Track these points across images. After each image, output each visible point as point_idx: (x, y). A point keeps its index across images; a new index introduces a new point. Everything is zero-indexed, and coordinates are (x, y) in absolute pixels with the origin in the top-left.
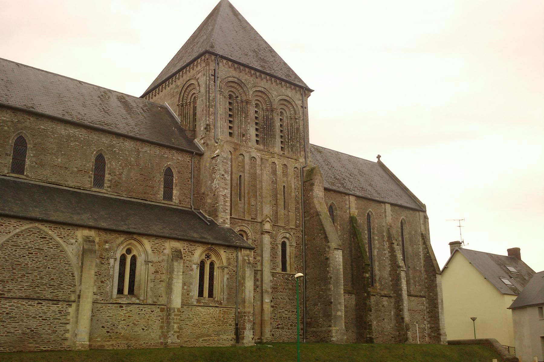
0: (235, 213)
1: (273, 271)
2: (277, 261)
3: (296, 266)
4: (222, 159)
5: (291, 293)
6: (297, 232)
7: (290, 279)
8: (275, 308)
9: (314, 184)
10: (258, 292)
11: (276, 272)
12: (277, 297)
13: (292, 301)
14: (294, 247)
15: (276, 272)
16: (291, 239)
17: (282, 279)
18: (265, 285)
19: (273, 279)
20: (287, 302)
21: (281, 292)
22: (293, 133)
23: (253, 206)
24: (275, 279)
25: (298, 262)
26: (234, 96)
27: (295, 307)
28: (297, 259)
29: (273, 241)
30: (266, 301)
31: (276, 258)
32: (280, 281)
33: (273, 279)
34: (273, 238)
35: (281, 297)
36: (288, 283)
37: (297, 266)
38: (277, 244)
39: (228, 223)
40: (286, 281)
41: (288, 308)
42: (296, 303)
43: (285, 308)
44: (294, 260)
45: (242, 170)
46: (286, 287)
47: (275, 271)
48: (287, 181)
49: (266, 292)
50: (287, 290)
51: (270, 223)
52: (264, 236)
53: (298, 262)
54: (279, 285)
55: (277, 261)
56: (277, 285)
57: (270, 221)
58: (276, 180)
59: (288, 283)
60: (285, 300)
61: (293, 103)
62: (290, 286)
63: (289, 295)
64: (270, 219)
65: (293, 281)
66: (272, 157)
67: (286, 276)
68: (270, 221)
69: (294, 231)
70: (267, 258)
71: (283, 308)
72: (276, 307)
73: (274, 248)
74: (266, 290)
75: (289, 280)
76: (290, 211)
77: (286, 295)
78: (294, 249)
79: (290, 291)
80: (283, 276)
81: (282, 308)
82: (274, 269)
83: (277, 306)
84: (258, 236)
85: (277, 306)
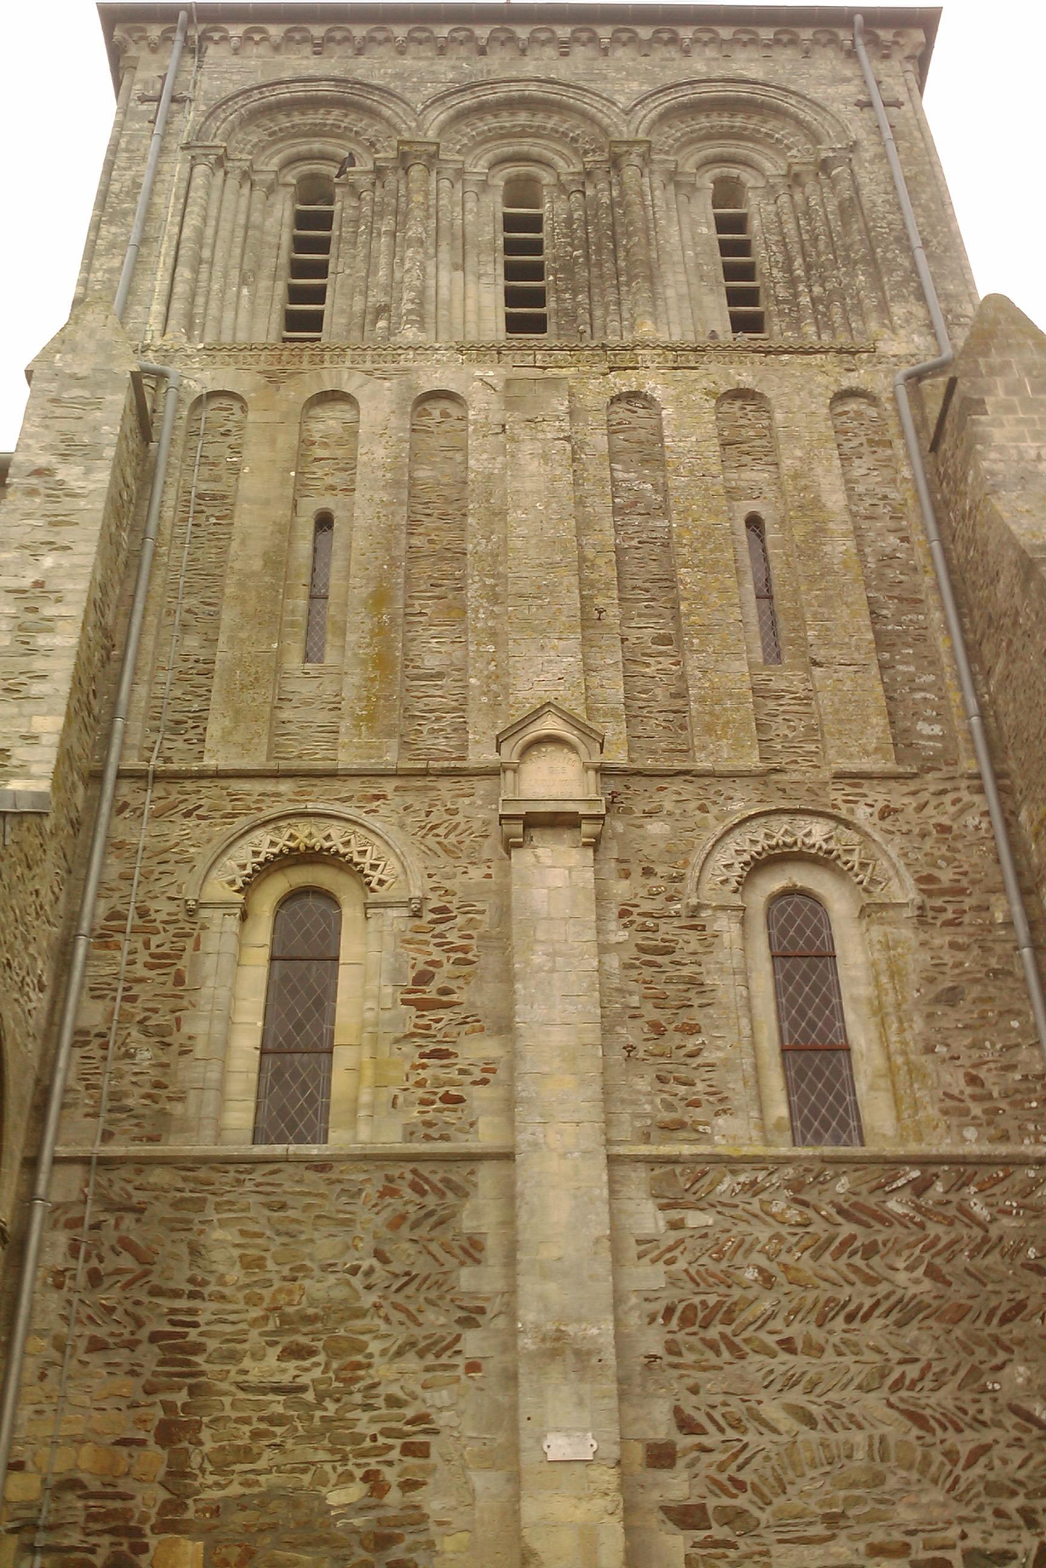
0: (238, 737)
1: (666, 1150)
2: (707, 1056)
3: (955, 1080)
4: (53, 386)
5: (926, 1351)
6: (925, 796)
7: (894, 1205)
8: (719, 1532)
9: (982, 402)
10: (473, 1367)
11: (696, 1159)
12: (736, 1407)
13: (965, 1443)
14: (908, 912)
15: (703, 1149)
16: (855, 859)
17: (793, 1214)
18: (551, 1287)
19: (676, 1225)
20: (881, 1449)
21: (788, 1345)
22: (815, 240)
23: (440, 675)
24: (695, 1219)
25: (977, 1045)
26: (332, 170)
27: (1012, 1505)
28: (950, 1018)
29: (652, 895)
30: (558, 1447)
31: (693, 1030)
32: (763, 1234)
33: (675, 1225)
34: (648, 872)
35: (796, 1396)
36: (871, 1250)
37: (973, 1080)
38: (695, 911)
39: (35, 769)
40: (847, 1229)
41: (906, 1515)
42: (1017, 1456)
43: (871, 1518)
44: (919, 1024)
45: (338, 479)
46: (861, 1296)
47: (686, 1150)
48: (778, 482)
49: (554, 1354)
50: (876, 1323)
51: (573, 748)
52: (522, 858)
53: (977, 1045)
54: (750, 1274)
55: (707, 1056)
56: (727, 1280)
57: (571, 735)
58: (663, 490)
59: (871, 1250)
60: (859, 1438)
61: (791, 104)
62: (902, 1277)
63: (912, 1371)
64: (570, 719)
65: (934, 1229)
66: (612, 369)
67: (842, 1185)
68: (571, 735)
69: (879, 795)
70: (559, 1037)
71: (832, 1520)
72: (733, 1517)
73: (669, 951)
74: (560, 1336)
75: (885, 1219)
76: (820, 655)
77: (859, 1373)
78: (906, 933)
79: (911, 1332)
80: (796, 1186)
81: (819, 1530)
82: (680, 1125)
83: (742, 1501)
84: (476, 874)
85: (742, 1501)
